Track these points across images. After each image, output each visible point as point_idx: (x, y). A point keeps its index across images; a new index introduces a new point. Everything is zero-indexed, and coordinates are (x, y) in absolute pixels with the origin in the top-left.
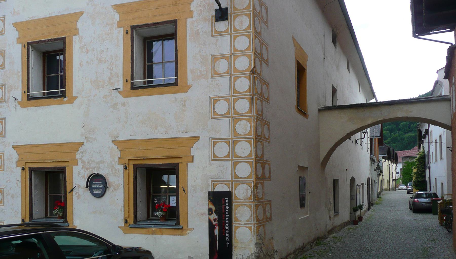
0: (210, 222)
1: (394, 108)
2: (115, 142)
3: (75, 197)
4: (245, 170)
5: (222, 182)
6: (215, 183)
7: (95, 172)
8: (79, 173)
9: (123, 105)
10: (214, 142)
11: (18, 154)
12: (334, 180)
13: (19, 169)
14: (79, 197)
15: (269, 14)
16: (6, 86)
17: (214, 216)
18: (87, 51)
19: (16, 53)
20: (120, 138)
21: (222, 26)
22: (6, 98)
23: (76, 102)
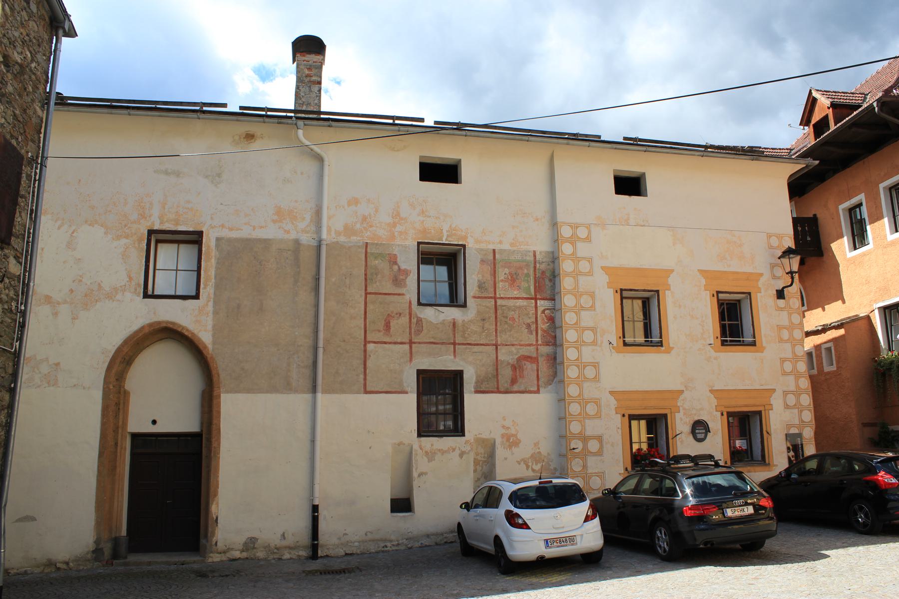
0: (789, 458)
1: (193, 145)
2: (711, 391)
3: (679, 443)
4: (808, 416)
5: (793, 426)
6: (789, 426)
7: (696, 418)
8: (681, 419)
9: (716, 359)
10: (786, 393)
11: (617, 400)
12: (423, 177)
13: (619, 416)
14: (682, 442)
15: (203, 249)
16: (598, 330)
17: (792, 453)
18: (680, 306)
19: (643, 171)
20: (715, 388)
21: (781, 302)
22: (599, 342)
23: (673, 352)
